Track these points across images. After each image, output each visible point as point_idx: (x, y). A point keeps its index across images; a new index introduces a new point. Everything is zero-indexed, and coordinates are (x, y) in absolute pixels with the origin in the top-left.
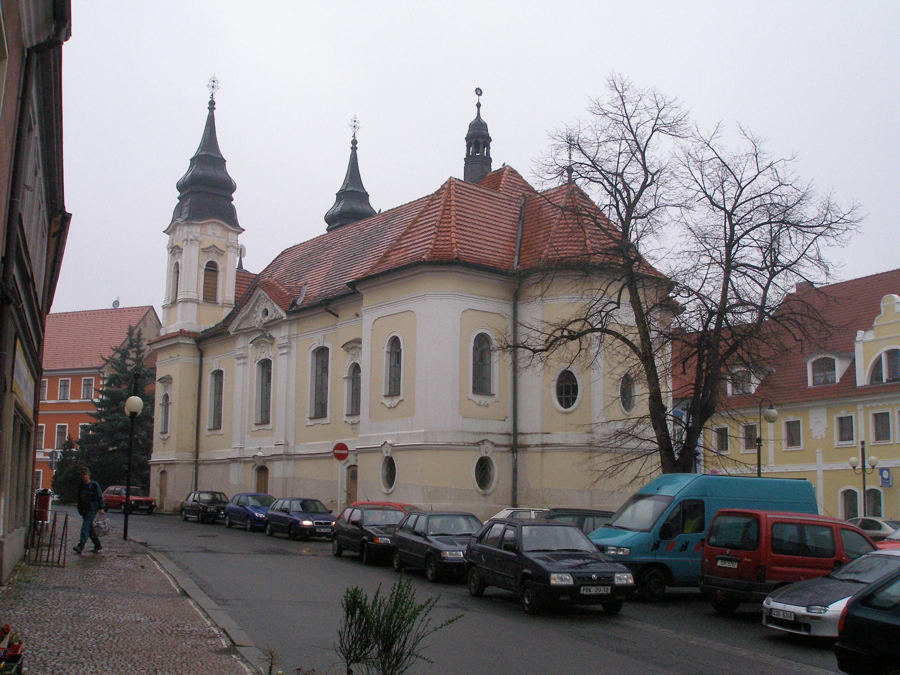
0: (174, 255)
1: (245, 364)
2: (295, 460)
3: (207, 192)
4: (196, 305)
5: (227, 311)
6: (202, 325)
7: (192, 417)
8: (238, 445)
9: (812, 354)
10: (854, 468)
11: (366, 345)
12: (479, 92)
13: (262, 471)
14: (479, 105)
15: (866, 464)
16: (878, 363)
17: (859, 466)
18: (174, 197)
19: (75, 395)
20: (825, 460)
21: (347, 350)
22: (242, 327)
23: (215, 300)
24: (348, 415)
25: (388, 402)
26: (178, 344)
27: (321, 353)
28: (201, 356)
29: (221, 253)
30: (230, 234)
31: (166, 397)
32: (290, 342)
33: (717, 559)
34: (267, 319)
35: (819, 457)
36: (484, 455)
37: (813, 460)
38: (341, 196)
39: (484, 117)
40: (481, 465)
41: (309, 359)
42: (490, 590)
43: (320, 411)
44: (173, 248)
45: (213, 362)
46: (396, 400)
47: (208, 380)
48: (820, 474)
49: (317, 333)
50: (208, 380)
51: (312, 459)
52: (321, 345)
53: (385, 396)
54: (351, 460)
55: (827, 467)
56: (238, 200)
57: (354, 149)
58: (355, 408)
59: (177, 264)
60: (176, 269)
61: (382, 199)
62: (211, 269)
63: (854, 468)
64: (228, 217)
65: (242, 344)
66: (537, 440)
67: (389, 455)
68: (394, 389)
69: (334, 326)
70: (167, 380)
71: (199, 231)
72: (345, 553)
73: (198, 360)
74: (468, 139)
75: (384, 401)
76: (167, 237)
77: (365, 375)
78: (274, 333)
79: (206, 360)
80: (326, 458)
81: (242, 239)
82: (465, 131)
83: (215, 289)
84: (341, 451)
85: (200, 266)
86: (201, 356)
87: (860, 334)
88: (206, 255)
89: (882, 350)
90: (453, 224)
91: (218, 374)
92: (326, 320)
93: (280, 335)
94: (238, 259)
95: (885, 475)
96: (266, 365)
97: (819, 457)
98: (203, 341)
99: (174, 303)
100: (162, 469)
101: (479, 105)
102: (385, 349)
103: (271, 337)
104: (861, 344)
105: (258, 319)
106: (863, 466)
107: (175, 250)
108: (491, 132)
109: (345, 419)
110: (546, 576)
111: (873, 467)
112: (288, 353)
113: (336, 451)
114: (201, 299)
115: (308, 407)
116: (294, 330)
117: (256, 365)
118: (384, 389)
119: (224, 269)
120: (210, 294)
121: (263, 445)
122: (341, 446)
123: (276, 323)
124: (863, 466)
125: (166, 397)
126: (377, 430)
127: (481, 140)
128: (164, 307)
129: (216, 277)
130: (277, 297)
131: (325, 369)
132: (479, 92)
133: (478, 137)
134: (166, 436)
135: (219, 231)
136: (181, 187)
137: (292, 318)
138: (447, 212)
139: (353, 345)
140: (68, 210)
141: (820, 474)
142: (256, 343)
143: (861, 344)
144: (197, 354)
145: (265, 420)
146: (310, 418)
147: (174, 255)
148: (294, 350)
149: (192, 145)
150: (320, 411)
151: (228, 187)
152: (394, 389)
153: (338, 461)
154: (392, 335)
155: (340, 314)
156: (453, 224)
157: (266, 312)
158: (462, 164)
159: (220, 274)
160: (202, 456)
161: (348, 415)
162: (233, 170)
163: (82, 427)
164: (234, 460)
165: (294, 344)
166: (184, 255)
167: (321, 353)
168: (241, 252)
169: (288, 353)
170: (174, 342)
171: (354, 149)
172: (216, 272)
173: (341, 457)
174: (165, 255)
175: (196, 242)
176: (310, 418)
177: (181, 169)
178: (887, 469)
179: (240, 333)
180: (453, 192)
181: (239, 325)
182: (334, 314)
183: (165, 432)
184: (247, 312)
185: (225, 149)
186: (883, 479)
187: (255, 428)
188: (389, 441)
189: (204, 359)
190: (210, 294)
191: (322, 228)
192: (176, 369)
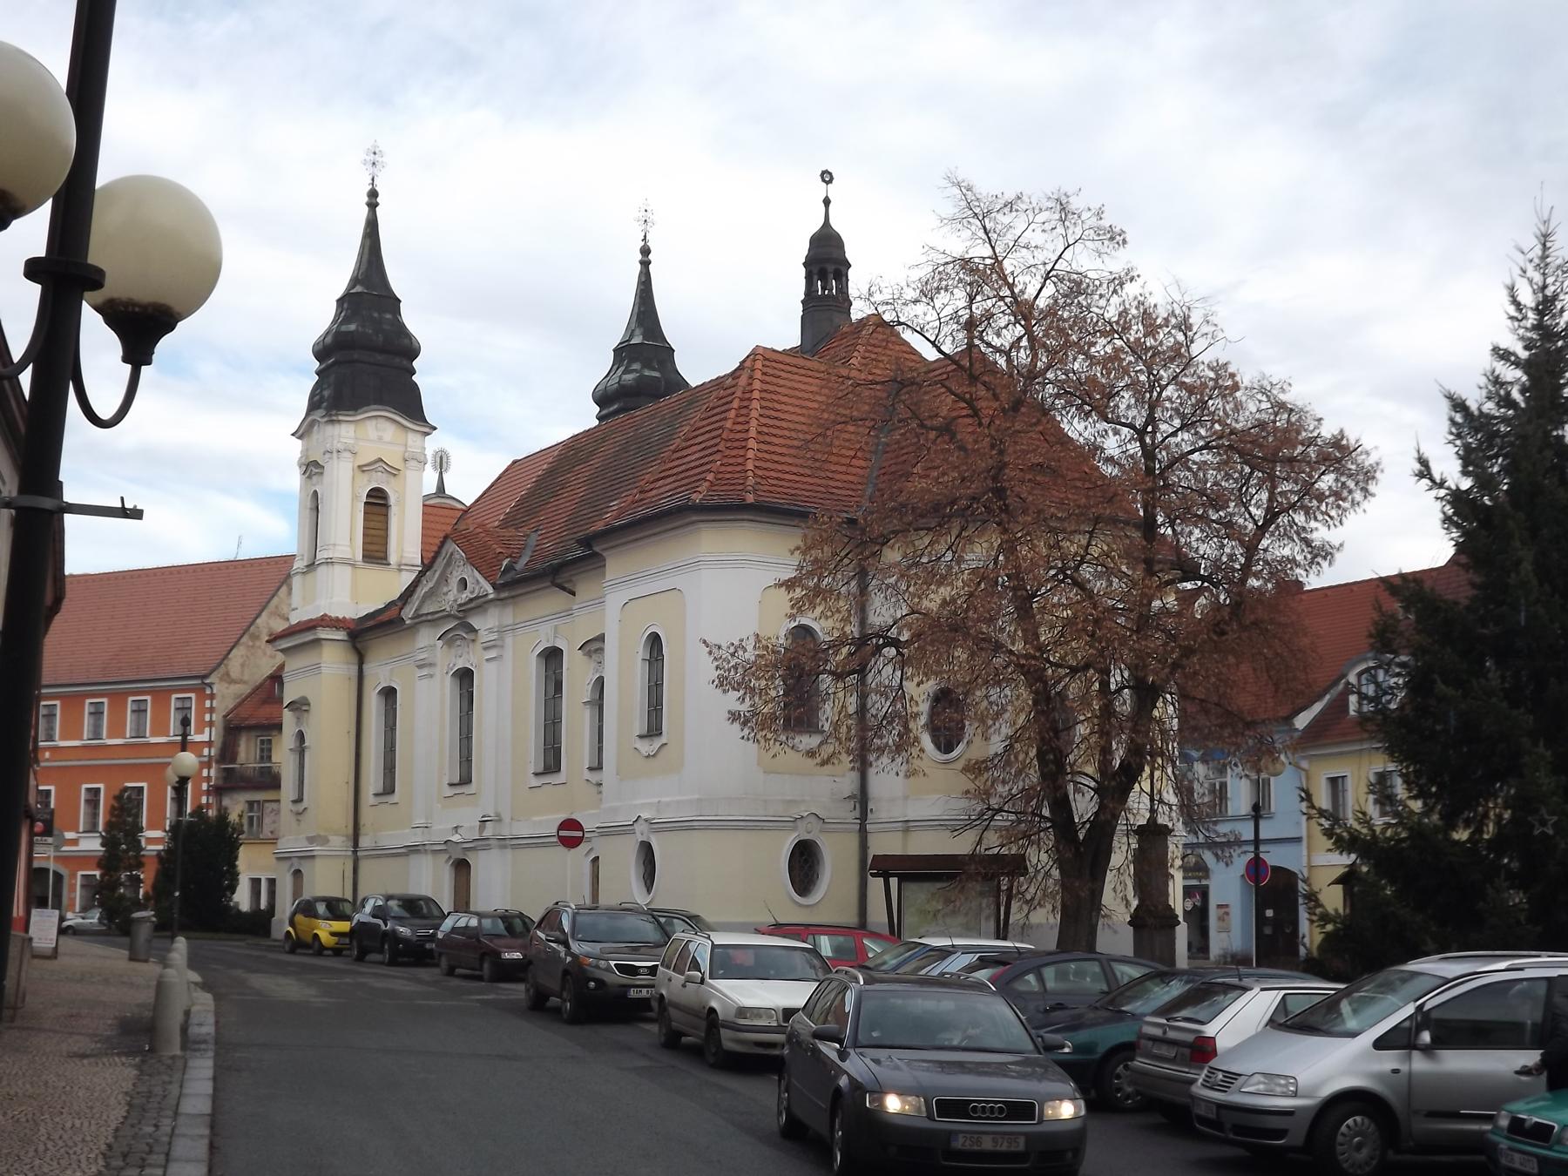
0: (310, 477)
2: (514, 847)
3: (367, 359)
4: (349, 568)
5: (408, 578)
8: (420, 821)
9: (1354, 665)
11: (610, 646)
12: (827, 178)
13: (462, 867)
14: (827, 202)
19: (117, 730)
21: (589, 654)
22: (425, 611)
23: (385, 558)
25: (646, 747)
26: (318, 640)
27: (552, 656)
28: (361, 663)
30: (411, 436)
32: (501, 639)
34: (465, 596)
38: (624, 353)
39: (836, 224)
41: (532, 668)
42: (459, 971)
43: (552, 763)
45: (380, 673)
46: (657, 743)
47: (373, 704)
49: (541, 622)
50: (373, 704)
51: (537, 845)
53: (641, 737)
56: (426, 375)
57: (645, 264)
60: (314, 504)
61: (700, 362)
62: (377, 503)
64: (408, 405)
65: (427, 638)
69: (568, 613)
70: (300, 706)
71: (352, 434)
72: (459, 971)
75: (640, 744)
78: (475, 622)
79: (368, 668)
80: (544, 845)
82: (803, 250)
83: (385, 538)
84: (570, 834)
85: (355, 497)
86: (361, 663)
88: (366, 477)
90: (753, 433)
91: (389, 694)
92: (553, 601)
93: (485, 623)
96: (465, 677)
98: (364, 634)
101: (827, 202)
102: (640, 656)
105: (452, 597)
107: (311, 468)
108: (850, 254)
110: (498, 954)
113: (563, 833)
115: (533, 756)
117: (448, 678)
118: (639, 725)
120: (375, 551)
121: (455, 820)
123: (478, 605)
125: (301, 736)
126: (634, 795)
127: (831, 268)
129: (386, 515)
130: (480, 560)
132: (827, 178)
133: (826, 260)
134: (300, 807)
137: (503, 595)
138: (744, 411)
139: (593, 648)
142: (447, 639)
144: (354, 659)
146: (536, 774)
147: (310, 477)
148: (508, 654)
149: (338, 276)
150: (552, 763)
151: (408, 350)
152: (654, 729)
155: (579, 589)
156: (753, 433)
158: (798, 310)
159: (394, 512)
160: (365, 842)
163: (88, 790)
164: (413, 850)
165: (509, 640)
167: (552, 656)
170: (309, 637)
171: (645, 264)
172: (386, 506)
173: (571, 843)
175: (347, 454)
176: (536, 774)
177: (320, 316)
179: (421, 620)
180: (758, 375)
182: (564, 589)
183: (299, 800)
184: (431, 585)
185: (398, 280)
187: (449, 792)
188: (645, 815)
190: (375, 551)
191: (586, 417)
192: (323, 679)
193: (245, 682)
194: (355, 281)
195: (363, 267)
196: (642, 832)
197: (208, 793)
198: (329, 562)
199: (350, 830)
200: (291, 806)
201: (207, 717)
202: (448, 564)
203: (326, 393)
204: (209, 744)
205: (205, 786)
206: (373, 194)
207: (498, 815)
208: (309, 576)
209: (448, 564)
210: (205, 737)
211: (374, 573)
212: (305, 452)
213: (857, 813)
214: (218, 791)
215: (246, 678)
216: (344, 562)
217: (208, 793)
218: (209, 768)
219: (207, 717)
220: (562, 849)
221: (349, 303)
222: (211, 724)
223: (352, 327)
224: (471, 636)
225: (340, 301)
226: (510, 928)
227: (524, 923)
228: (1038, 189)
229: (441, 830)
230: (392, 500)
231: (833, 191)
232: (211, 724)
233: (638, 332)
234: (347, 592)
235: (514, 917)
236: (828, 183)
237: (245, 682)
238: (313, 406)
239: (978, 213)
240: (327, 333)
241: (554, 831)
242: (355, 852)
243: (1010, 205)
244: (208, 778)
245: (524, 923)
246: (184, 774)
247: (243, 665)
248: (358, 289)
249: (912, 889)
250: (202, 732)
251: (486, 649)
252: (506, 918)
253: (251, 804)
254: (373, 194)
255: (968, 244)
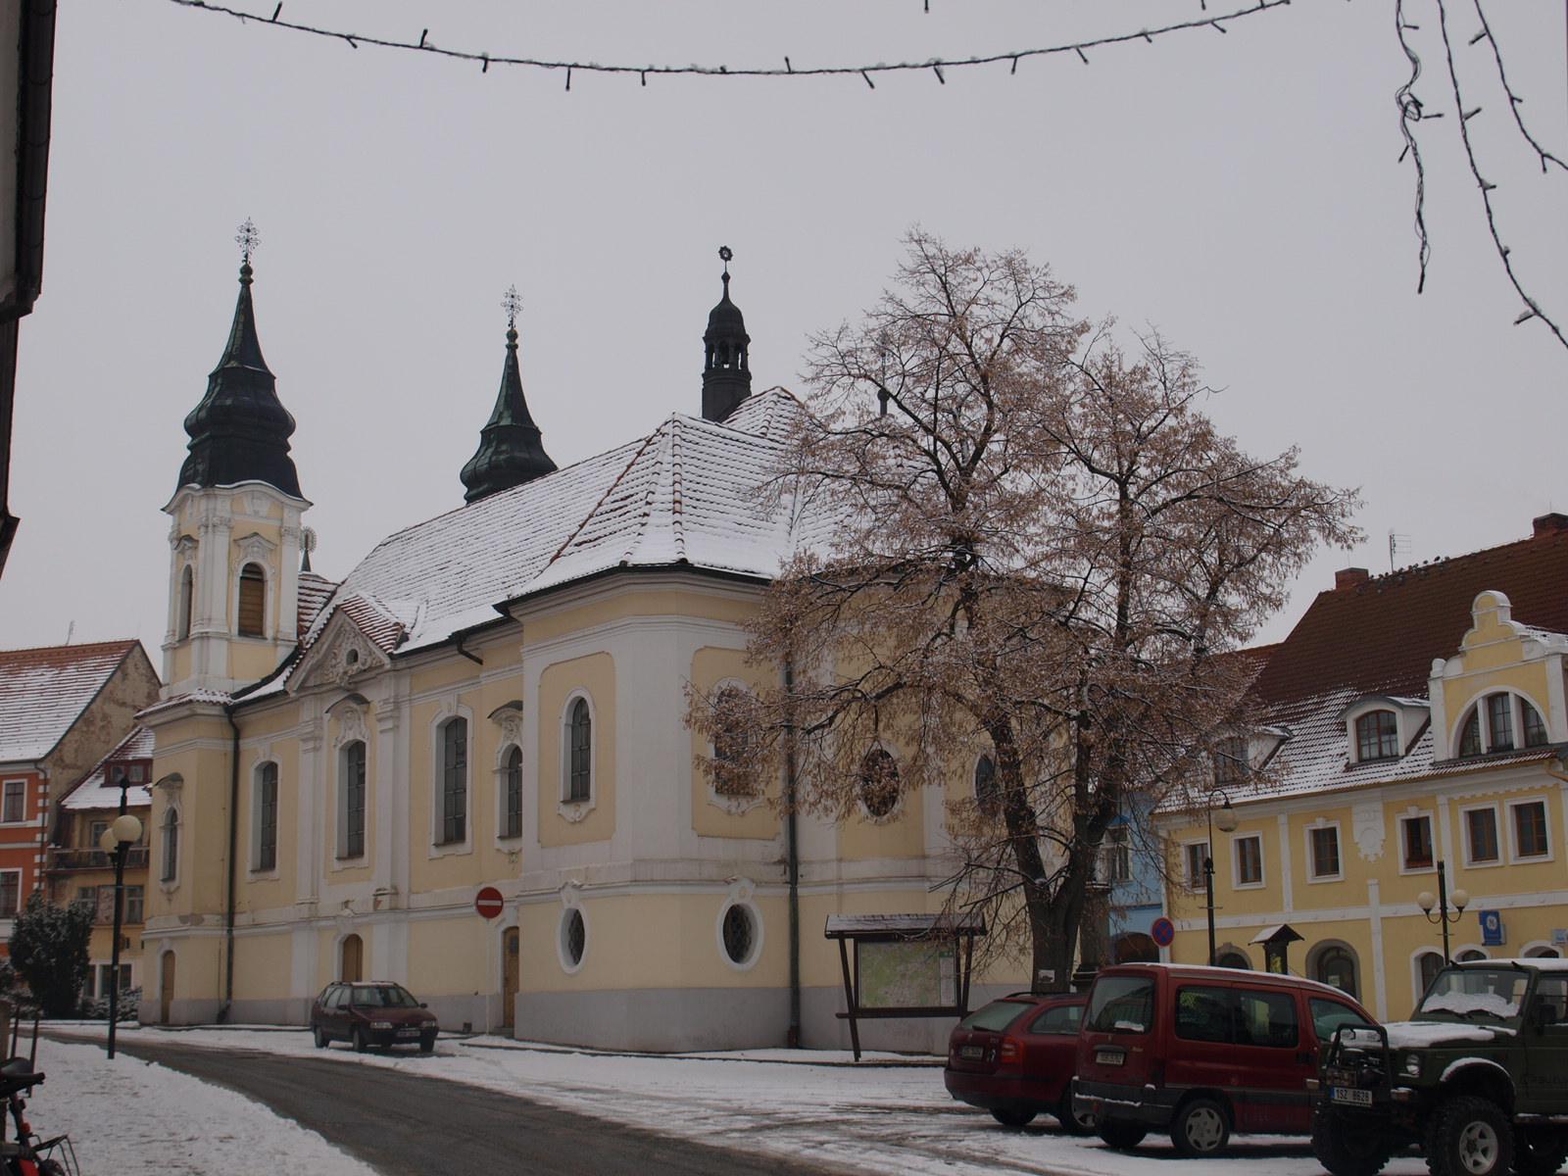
0: (182, 552)
1: (316, 749)
6: (237, 682)
7: (221, 872)
10: (1427, 911)
12: (726, 254)
14: (726, 278)
15: (1449, 904)
16: (1472, 717)
17: (1436, 910)
18: (180, 446)
20: (1384, 900)
24: (501, 838)
25: (570, 812)
27: (454, 730)
28: (237, 736)
29: (274, 549)
31: (173, 815)
33: (1096, 1052)
35: (1373, 893)
36: (738, 901)
37: (1363, 900)
39: (734, 300)
40: (734, 919)
41: (432, 743)
43: (453, 830)
44: (180, 540)
45: (257, 749)
46: (584, 808)
48: (1376, 926)
52: (452, 714)
54: (507, 917)
55: (1387, 911)
56: (299, 449)
57: (512, 348)
58: (513, 827)
59: (189, 571)
62: (253, 579)
63: (1427, 911)
64: (286, 479)
66: (830, 872)
67: (573, 906)
68: (579, 791)
73: (230, 745)
74: (708, 338)
76: (168, 520)
77: (528, 766)
79: (244, 744)
81: (307, 519)
85: (231, 572)
87: (1438, 664)
89: (1478, 697)
91: (269, 771)
94: (301, 555)
95: (1491, 921)
96: (356, 753)
97: (1373, 893)
98: (236, 714)
99: (185, 638)
100: (167, 948)
101: (726, 278)
102: (563, 721)
103: (363, 701)
104: (1439, 683)
106: (1444, 908)
107: (183, 542)
108: (749, 328)
109: (498, 844)
111: (1461, 909)
112: (396, 728)
114: (235, 629)
116: (405, 685)
117: (337, 752)
118: (561, 787)
119: (278, 575)
120: (251, 624)
122: (489, 893)
124: (1444, 908)
127: (731, 342)
128: (165, 649)
131: (461, 753)
132: (726, 254)
134: (173, 885)
135: (264, 507)
136: (193, 426)
140: (13, 512)
141: (1376, 926)
143: (1439, 683)
144: (229, 733)
145: (354, 847)
147: (182, 552)
148: (405, 724)
150: (453, 830)
151: (283, 424)
152: (579, 791)
153: (484, 920)
154: (573, 696)
157: (354, 656)
159: (270, 585)
161: (501, 838)
162: (287, 394)
166: (201, 554)
167: (454, 730)
168: (307, 541)
169: (316, 749)
171: (512, 348)
173: (489, 913)
174: (165, 552)
176: (339, 858)
177: (193, 392)
178: (1495, 913)
181: (305, 681)
186: (1486, 930)
189: (241, 742)
190: (251, 624)
193: (79, 768)
194: (228, 356)
195: (238, 342)
196: (570, 901)
197: (40, 879)
198: (205, 637)
199: (226, 909)
200: (161, 885)
201: (40, 803)
202: (337, 636)
203: (200, 468)
204: (42, 830)
205: (37, 872)
206: (247, 271)
207: (394, 887)
208: (181, 652)
209: (337, 636)
210: (37, 823)
211: (249, 644)
212: (178, 527)
213: (787, 877)
214: (53, 878)
215: (79, 764)
216: (220, 636)
217: (40, 879)
218: (42, 854)
219: (40, 803)
220: (482, 920)
221: (221, 378)
222: (44, 809)
223: (229, 402)
224: (365, 706)
225: (213, 377)
226: (387, 1002)
227: (399, 995)
228: (993, 248)
229: (330, 900)
230: (269, 574)
231: (732, 267)
232: (44, 809)
233: (506, 414)
234: (221, 670)
235: (389, 988)
236: (726, 259)
237: (79, 768)
238: (185, 479)
239: (941, 269)
240: (200, 408)
241: (473, 900)
242: (230, 931)
243: (968, 260)
244: (41, 865)
245: (399, 995)
246: (126, 838)
247: (76, 751)
248: (233, 364)
249: (867, 949)
250: (35, 818)
251: (380, 720)
252: (383, 990)
253: (84, 892)
254: (247, 271)
255: (921, 298)
